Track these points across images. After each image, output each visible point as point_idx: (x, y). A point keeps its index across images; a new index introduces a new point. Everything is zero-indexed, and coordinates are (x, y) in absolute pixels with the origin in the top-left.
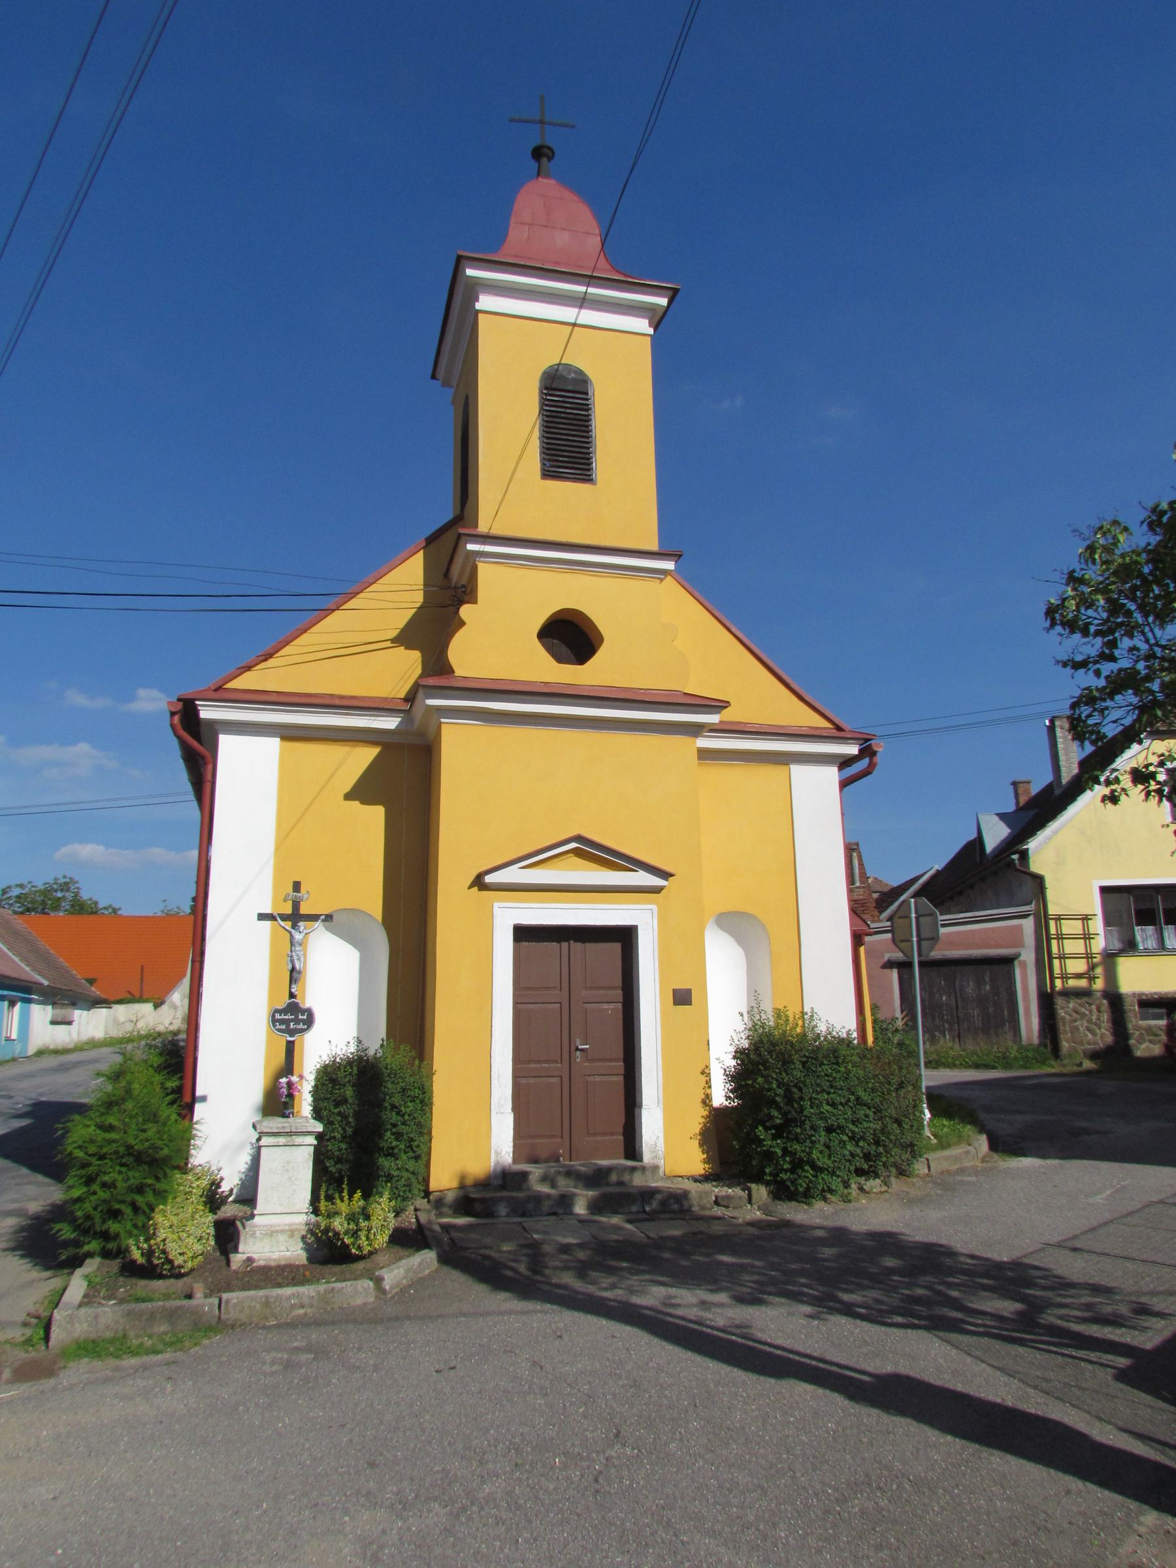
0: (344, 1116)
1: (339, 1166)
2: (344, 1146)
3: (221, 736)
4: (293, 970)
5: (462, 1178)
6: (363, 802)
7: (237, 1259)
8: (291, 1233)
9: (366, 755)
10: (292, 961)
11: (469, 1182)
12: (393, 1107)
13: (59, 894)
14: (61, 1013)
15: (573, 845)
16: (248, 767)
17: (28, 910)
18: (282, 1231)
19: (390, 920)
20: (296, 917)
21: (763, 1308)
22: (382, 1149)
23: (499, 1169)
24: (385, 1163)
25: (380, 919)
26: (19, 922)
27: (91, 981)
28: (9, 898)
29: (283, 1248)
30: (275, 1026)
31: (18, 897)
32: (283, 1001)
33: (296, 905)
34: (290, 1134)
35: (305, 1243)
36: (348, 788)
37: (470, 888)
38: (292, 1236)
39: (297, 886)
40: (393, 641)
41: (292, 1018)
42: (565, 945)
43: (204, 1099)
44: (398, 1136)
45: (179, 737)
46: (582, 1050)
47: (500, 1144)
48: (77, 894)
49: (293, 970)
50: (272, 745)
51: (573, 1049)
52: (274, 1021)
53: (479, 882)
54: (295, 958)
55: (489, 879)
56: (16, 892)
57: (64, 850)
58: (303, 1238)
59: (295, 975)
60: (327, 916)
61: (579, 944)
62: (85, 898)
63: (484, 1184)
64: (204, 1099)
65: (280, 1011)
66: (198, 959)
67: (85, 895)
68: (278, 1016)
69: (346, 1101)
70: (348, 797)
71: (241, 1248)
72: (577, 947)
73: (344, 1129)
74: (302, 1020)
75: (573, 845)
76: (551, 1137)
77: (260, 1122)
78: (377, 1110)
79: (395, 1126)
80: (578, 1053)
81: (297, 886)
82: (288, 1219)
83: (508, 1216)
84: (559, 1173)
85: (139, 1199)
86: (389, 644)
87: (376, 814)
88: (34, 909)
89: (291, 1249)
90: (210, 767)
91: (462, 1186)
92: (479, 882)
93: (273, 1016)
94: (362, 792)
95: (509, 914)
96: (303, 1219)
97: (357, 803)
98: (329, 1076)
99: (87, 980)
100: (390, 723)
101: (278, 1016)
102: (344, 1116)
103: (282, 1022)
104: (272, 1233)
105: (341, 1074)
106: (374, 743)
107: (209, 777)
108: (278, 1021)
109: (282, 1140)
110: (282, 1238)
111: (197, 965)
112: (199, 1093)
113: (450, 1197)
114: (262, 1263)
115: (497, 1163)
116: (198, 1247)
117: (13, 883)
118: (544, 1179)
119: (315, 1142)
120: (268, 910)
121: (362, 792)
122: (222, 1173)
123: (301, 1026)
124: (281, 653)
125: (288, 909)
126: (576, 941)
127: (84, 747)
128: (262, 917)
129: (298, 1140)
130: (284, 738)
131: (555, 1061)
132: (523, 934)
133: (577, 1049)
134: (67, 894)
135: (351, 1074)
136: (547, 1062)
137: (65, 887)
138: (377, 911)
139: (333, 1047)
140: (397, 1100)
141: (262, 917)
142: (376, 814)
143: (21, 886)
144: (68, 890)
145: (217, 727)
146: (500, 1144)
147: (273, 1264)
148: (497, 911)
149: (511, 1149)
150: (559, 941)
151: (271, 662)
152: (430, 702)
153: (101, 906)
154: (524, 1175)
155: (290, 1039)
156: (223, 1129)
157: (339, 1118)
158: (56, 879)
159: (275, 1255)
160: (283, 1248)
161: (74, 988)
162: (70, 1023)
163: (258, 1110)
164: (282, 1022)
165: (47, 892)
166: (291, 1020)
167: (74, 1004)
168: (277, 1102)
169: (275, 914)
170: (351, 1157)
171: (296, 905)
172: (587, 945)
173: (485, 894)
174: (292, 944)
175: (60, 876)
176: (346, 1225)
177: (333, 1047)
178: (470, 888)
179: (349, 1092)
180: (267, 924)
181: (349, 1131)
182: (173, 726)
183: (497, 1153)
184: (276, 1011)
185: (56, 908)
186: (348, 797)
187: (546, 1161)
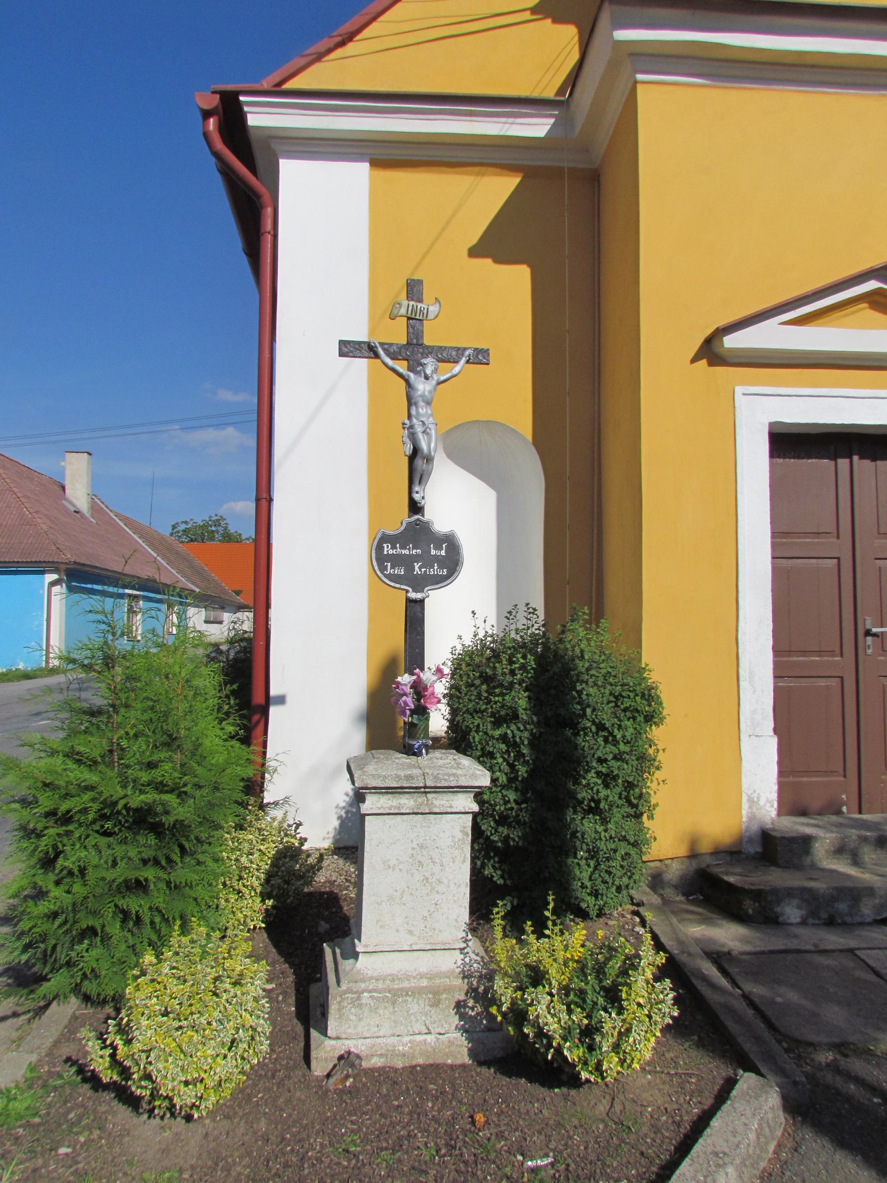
0: (512, 744)
1: (503, 830)
2: (512, 796)
3: (281, 161)
4: (416, 451)
5: (693, 843)
6: (498, 260)
7: (325, 1051)
8: (434, 995)
9: (497, 189)
10: (413, 437)
11: (705, 847)
12: (601, 727)
13: (214, 528)
14: (212, 614)
15: (873, 285)
16: (322, 211)
17: (192, 540)
18: (415, 992)
19: (545, 438)
20: (413, 351)
21: (835, 885)
22: (581, 802)
23: (755, 828)
24: (588, 826)
25: (529, 435)
26: (181, 548)
27: (238, 593)
28: (178, 532)
29: (419, 1027)
30: (383, 569)
31: (184, 531)
32: (398, 520)
33: (414, 322)
34: (425, 790)
35: (462, 1016)
36: (474, 239)
37: (694, 360)
38: (436, 1004)
39: (414, 289)
40: (534, 10)
41: (413, 555)
42: (843, 463)
43: (281, 700)
44: (608, 779)
45: (216, 155)
46: (875, 635)
47: (757, 789)
48: (226, 528)
49: (416, 451)
50: (357, 174)
51: (861, 633)
52: (380, 559)
53: (710, 351)
54: (419, 429)
55: (731, 342)
56: (183, 527)
57: (225, 506)
58: (459, 1006)
59: (419, 463)
60: (478, 351)
61: (867, 463)
62: (232, 531)
63: (733, 853)
64: (281, 700)
65: (392, 540)
66: (265, 495)
67: (232, 530)
68: (387, 549)
69: (515, 717)
70: (475, 252)
71: (333, 1025)
72: (863, 466)
73: (512, 766)
74: (437, 559)
75: (873, 285)
76: (826, 773)
77: (361, 762)
78: (569, 732)
79: (601, 761)
80: (869, 639)
81: (414, 289)
82: (425, 963)
83: (803, 923)
84: (865, 839)
85: (133, 903)
86: (527, 16)
87: (519, 277)
88: (196, 540)
89: (435, 1029)
90: (269, 210)
91: (693, 855)
92: (710, 351)
93: (379, 548)
94: (495, 245)
95: (762, 406)
96: (450, 962)
97: (488, 262)
98: (477, 671)
99: (234, 592)
100: (536, 127)
101: (387, 549)
102: (512, 744)
103: (396, 560)
104: (396, 994)
105: (502, 668)
106: (511, 168)
107: (269, 227)
108: (390, 558)
109: (407, 802)
110: (415, 1006)
111: (264, 503)
112: (273, 692)
113: (674, 872)
114: (377, 1062)
115: (752, 818)
116: (222, 1068)
117: (180, 521)
118: (840, 850)
119: (475, 808)
120: (361, 335)
121: (495, 245)
122: (302, 832)
123: (435, 570)
124: (366, 33)
125: (398, 335)
126: (862, 457)
127: (230, 431)
128: (347, 349)
129: (440, 802)
130: (376, 164)
131: (832, 653)
132: (787, 442)
133: (868, 633)
134: (219, 528)
135: (523, 667)
136: (819, 653)
137: (217, 523)
138: (526, 428)
139: (480, 623)
140: (606, 716)
141: (347, 349)
142: (519, 277)
143: (186, 523)
144: (219, 525)
145: (275, 146)
146: (757, 789)
147: (399, 1064)
148: (740, 400)
149: (775, 796)
150: (834, 457)
151: (351, 48)
152: (623, 35)
153: (244, 537)
154: (805, 842)
155: (413, 595)
156: (310, 754)
157: (503, 747)
158: (210, 517)
159: (403, 1044)
160: (419, 1027)
161: (222, 596)
162: (221, 622)
163: (360, 718)
164: (396, 560)
165: (205, 526)
166: (416, 558)
167: (223, 608)
168: (390, 721)
169: (375, 341)
170: (525, 817)
171: (414, 322)
172: (879, 463)
173: (720, 371)
174: (410, 402)
175: (213, 515)
176: (564, 1016)
177: (480, 623)
178: (694, 360)
179: (521, 701)
180: (361, 365)
181: (522, 771)
182: (206, 135)
183: (750, 800)
184: (385, 539)
185: (212, 539)
186: (475, 252)
187: (820, 814)
